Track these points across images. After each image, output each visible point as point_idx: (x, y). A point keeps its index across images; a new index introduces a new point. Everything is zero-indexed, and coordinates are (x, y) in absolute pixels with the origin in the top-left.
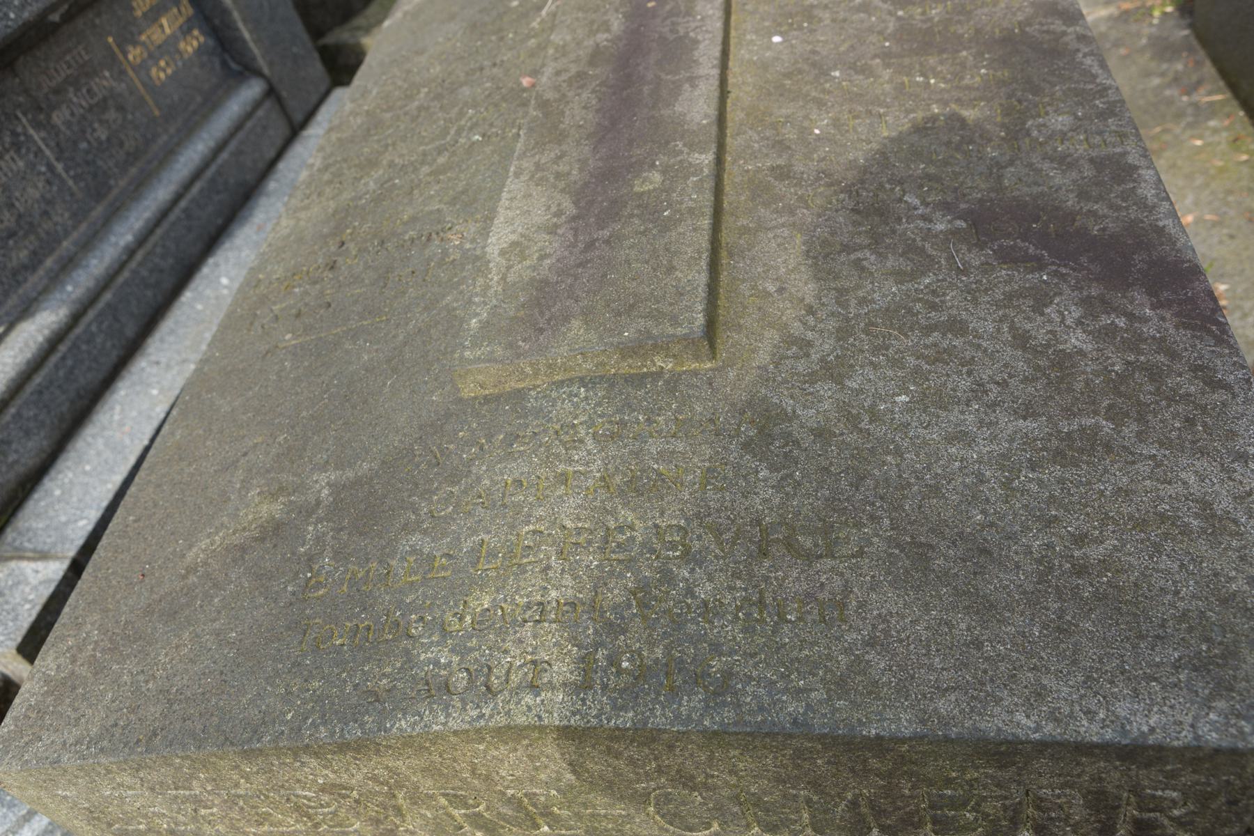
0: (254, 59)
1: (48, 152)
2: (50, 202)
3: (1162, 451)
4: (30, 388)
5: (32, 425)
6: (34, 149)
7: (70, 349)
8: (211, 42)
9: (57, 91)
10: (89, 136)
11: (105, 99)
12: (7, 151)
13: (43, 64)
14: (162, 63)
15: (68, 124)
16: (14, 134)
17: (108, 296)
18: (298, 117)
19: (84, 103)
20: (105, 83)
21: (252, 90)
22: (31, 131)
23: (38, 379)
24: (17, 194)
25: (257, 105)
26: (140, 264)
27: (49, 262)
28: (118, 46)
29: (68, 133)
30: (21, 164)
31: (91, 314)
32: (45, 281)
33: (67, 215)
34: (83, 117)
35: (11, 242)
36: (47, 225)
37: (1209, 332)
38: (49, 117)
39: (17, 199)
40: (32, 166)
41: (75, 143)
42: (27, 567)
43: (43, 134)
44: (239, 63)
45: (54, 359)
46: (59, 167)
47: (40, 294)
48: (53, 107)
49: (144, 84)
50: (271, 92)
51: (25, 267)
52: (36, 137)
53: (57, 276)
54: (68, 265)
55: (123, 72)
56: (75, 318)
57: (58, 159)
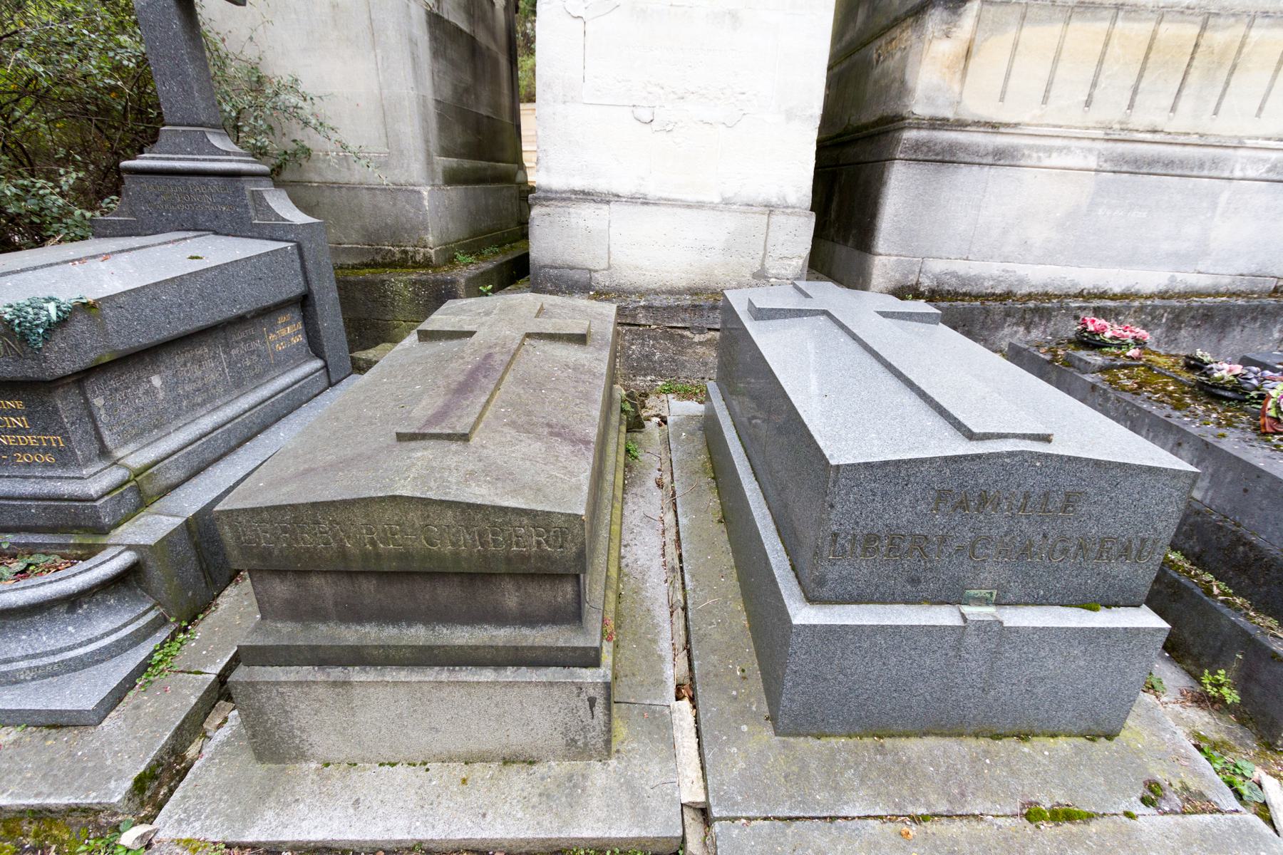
17: (229, 425)
18: (333, 381)
21: (318, 364)
25: (317, 371)
40: (216, 367)
42: (164, 518)
50: (326, 367)
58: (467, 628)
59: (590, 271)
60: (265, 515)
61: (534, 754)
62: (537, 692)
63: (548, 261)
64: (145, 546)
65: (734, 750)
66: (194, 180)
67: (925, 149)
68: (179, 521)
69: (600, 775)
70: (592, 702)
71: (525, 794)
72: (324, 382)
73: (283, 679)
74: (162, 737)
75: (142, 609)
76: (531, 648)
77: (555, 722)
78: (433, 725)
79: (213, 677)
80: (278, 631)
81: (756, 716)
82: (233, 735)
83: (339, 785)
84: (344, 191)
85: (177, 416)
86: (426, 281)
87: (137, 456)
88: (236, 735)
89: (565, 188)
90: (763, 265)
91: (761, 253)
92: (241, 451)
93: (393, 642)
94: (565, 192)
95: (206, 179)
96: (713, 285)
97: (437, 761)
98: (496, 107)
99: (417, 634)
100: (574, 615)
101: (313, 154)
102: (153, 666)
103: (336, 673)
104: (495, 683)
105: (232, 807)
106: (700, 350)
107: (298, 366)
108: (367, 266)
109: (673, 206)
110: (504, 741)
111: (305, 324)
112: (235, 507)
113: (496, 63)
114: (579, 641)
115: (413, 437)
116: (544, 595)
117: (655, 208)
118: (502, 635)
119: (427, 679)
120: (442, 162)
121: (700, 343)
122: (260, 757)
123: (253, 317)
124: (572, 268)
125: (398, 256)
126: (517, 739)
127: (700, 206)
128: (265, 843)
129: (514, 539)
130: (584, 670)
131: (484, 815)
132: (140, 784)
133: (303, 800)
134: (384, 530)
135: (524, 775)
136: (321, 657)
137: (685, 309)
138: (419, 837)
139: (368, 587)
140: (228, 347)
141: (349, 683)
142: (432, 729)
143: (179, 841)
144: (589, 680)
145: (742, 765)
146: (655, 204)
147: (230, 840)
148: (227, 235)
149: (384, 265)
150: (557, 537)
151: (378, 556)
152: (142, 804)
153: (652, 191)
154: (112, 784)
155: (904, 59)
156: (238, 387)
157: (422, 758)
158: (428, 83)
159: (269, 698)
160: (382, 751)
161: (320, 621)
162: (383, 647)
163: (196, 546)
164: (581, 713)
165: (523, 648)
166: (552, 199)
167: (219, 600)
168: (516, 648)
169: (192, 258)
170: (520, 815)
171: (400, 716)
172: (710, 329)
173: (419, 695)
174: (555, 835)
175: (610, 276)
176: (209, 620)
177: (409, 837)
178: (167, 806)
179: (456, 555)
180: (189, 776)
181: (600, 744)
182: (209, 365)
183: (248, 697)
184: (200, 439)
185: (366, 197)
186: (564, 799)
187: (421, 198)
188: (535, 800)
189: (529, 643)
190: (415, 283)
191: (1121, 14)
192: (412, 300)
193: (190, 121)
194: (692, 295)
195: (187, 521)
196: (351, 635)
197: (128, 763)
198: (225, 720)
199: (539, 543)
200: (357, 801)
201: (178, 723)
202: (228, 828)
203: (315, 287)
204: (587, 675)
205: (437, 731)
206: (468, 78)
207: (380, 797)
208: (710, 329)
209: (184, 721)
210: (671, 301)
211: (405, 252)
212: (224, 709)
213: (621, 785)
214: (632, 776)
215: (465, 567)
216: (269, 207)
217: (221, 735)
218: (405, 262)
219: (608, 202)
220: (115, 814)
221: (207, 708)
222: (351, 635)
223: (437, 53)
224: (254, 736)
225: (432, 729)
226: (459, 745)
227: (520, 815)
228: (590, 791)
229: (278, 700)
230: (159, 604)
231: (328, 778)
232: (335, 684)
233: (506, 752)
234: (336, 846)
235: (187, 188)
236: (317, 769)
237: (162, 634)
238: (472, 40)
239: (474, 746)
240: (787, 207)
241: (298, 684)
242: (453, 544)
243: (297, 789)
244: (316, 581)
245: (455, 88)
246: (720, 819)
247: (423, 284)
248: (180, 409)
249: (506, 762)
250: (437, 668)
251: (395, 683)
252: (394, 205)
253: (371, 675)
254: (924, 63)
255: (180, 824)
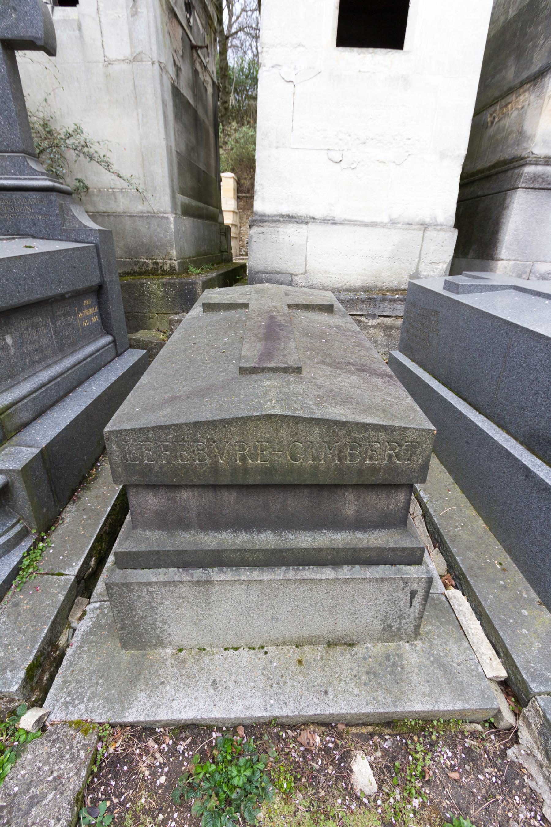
2: (48, 346)
8: (100, 321)
16: (46, 322)
17: (59, 379)
18: (119, 352)
21: (109, 339)
25: (109, 343)
31: (53, 383)
36: (46, 353)
42: (24, 449)
45: (40, 391)
46: (54, 337)
50: (114, 341)
54: (49, 366)
58: (309, 533)
59: (292, 275)
60: (151, 434)
61: (355, 638)
62: (369, 587)
63: (261, 268)
64: (13, 471)
65: (524, 631)
66: (17, 195)
67: (540, 180)
68: (36, 451)
69: (412, 654)
70: (413, 594)
71: (355, 672)
72: (113, 353)
73: (154, 579)
74: (42, 630)
75: (11, 523)
76: (368, 549)
77: (378, 611)
78: (275, 616)
79: (73, 578)
80: (148, 539)
81: (530, 601)
82: (94, 625)
83: (195, 668)
84: (112, 218)
85: (23, 370)
86: (174, 283)
88: (97, 626)
89: (275, 213)
90: (417, 269)
91: (417, 260)
92: (68, 400)
93: (248, 547)
94: (274, 216)
95: (27, 194)
96: (380, 284)
97: (273, 645)
98: (208, 165)
99: (267, 539)
100: (401, 521)
101: (90, 190)
102: (23, 570)
103: (198, 574)
104: (335, 580)
105: (109, 690)
106: (372, 331)
107: (97, 339)
108: (128, 274)
109: (354, 225)
110: (332, 627)
111: (100, 308)
112: (123, 427)
113: (208, 132)
114: (407, 543)
115: (253, 371)
116: (381, 502)
117: (341, 227)
118: (340, 539)
119: (276, 577)
120: (182, 199)
121: (373, 326)
122: (125, 645)
123: (73, 297)
124: (278, 273)
125: (151, 266)
126: (342, 625)
127: (374, 225)
128: (143, 722)
129: (369, 453)
130: (408, 567)
131: (326, 693)
132: (32, 672)
133: (169, 683)
134: (255, 447)
135: (348, 656)
136: (185, 560)
137: (363, 301)
138: (276, 714)
139: (229, 498)
140: (54, 319)
141: (211, 582)
142: (273, 619)
143: (71, 723)
144: (415, 576)
145: (537, 644)
146: (341, 224)
147: (113, 720)
148: (42, 238)
149: (141, 274)
150: (407, 450)
151: (246, 471)
152: (32, 691)
153: (339, 215)
154: (9, 675)
155: (521, 118)
156: (61, 351)
157: (260, 643)
158: (172, 137)
159: (139, 597)
160: (228, 638)
161: (183, 529)
162: (240, 550)
163: (48, 471)
164: (402, 603)
165: (360, 549)
166: (266, 222)
167: (63, 515)
168: (354, 550)
169: (26, 247)
170: (356, 692)
171: (249, 609)
172: (380, 316)
173: (268, 591)
174: (392, 709)
175: (306, 279)
176: (59, 531)
177: (268, 714)
178: (52, 691)
179: (315, 468)
180: (65, 662)
181: (411, 629)
182: (42, 332)
183: (121, 596)
184: (40, 388)
185: (128, 222)
186: (388, 677)
187: (169, 223)
188: (364, 677)
189: (364, 544)
190: (166, 285)
192: (163, 298)
193: (14, 148)
194: (365, 291)
195: (42, 451)
196: (211, 540)
197: (18, 655)
198: (85, 613)
199: (390, 456)
200: (214, 681)
201: (52, 618)
202: (109, 710)
203: (107, 279)
204: (412, 571)
205: (277, 620)
206: (193, 140)
207: (233, 678)
208: (380, 316)
209: (56, 617)
210: (351, 296)
211: (156, 263)
212: (81, 604)
213: (432, 663)
214: (438, 654)
215: (321, 480)
216: (74, 216)
217: (83, 626)
218: (156, 271)
219: (307, 223)
220: (13, 700)
221: (70, 603)
222: (211, 540)
223: (178, 117)
224: (122, 628)
225: (273, 619)
226: (294, 633)
227: (356, 692)
228: (408, 668)
229: (147, 598)
230: (23, 518)
231: (184, 662)
232: (198, 583)
233: (332, 637)
234: (203, 722)
235: (12, 201)
236: (173, 654)
237: (26, 544)
238: (195, 112)
239: (306, 633)
240: (437, 225)
241: (165, 584)
242: (314, 459)
243: (161, 672)
244: (184, 494)
245: (187, 145)
246: (540, 694)
247: (171, 285)
248: (25, 364)
249: (330, 644)
250: (283, 568)
251: (250, 582)
252: (149, 228)
253: (228, 575)
254: (543, 114)
255: (67, 707)
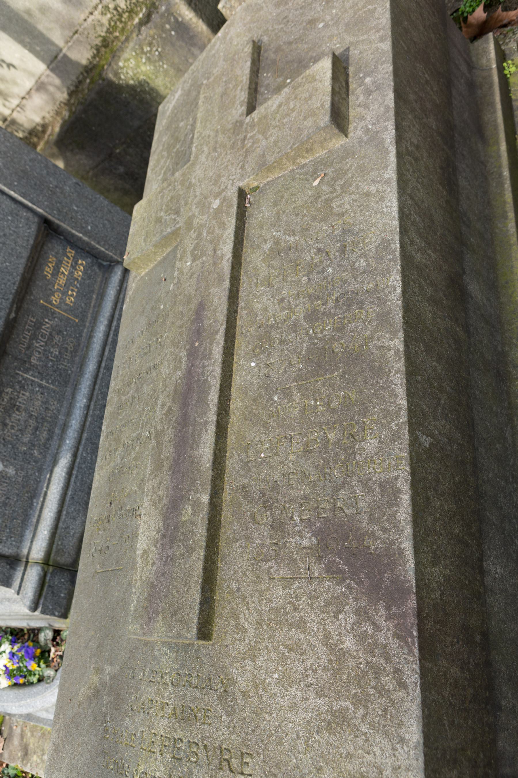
0: (112, 257)
1: (36, 380)
3: (370, 731)
4: (68, 499)
5: (75, 514)
6: (30, 383)
7: (78, 471)
8: (89, 260)
9: (28, 348)
10: (50, 358)
11: (51, 334)
12: (19, 392)
13: (17, 340)
14: (70, 292)
15: (39, 359)
16: (19, 382)
17: (85, 435)
19: (42, 344)
20: (48, 325)
22: (25, 375)
23: (69, 493)
24: (31, 409)
26: (94, 410)
27: (57, 431)
28: (46, 302)
29: (41, 363)
30: (27, 394)
32: (58, 441)
33: (56, 403)
34: (45, 350)
35: (38, 433)
37: (407, 643)
38: (30, 362)
39: (32, 411)
41: (46, 366)
43: (31, 373)
44: (107, 261)
45: (73, 479)
47: (58, 450)
48: (29, 357)
49: (65, 311)
51: (48, 440)
52: (29, 377)
53: (62, 436)
55: (54, 313)
56: (75, 456)
57: (41, 380)
87: (37, 548)
123: (18, 309)
191: (312, 576)
